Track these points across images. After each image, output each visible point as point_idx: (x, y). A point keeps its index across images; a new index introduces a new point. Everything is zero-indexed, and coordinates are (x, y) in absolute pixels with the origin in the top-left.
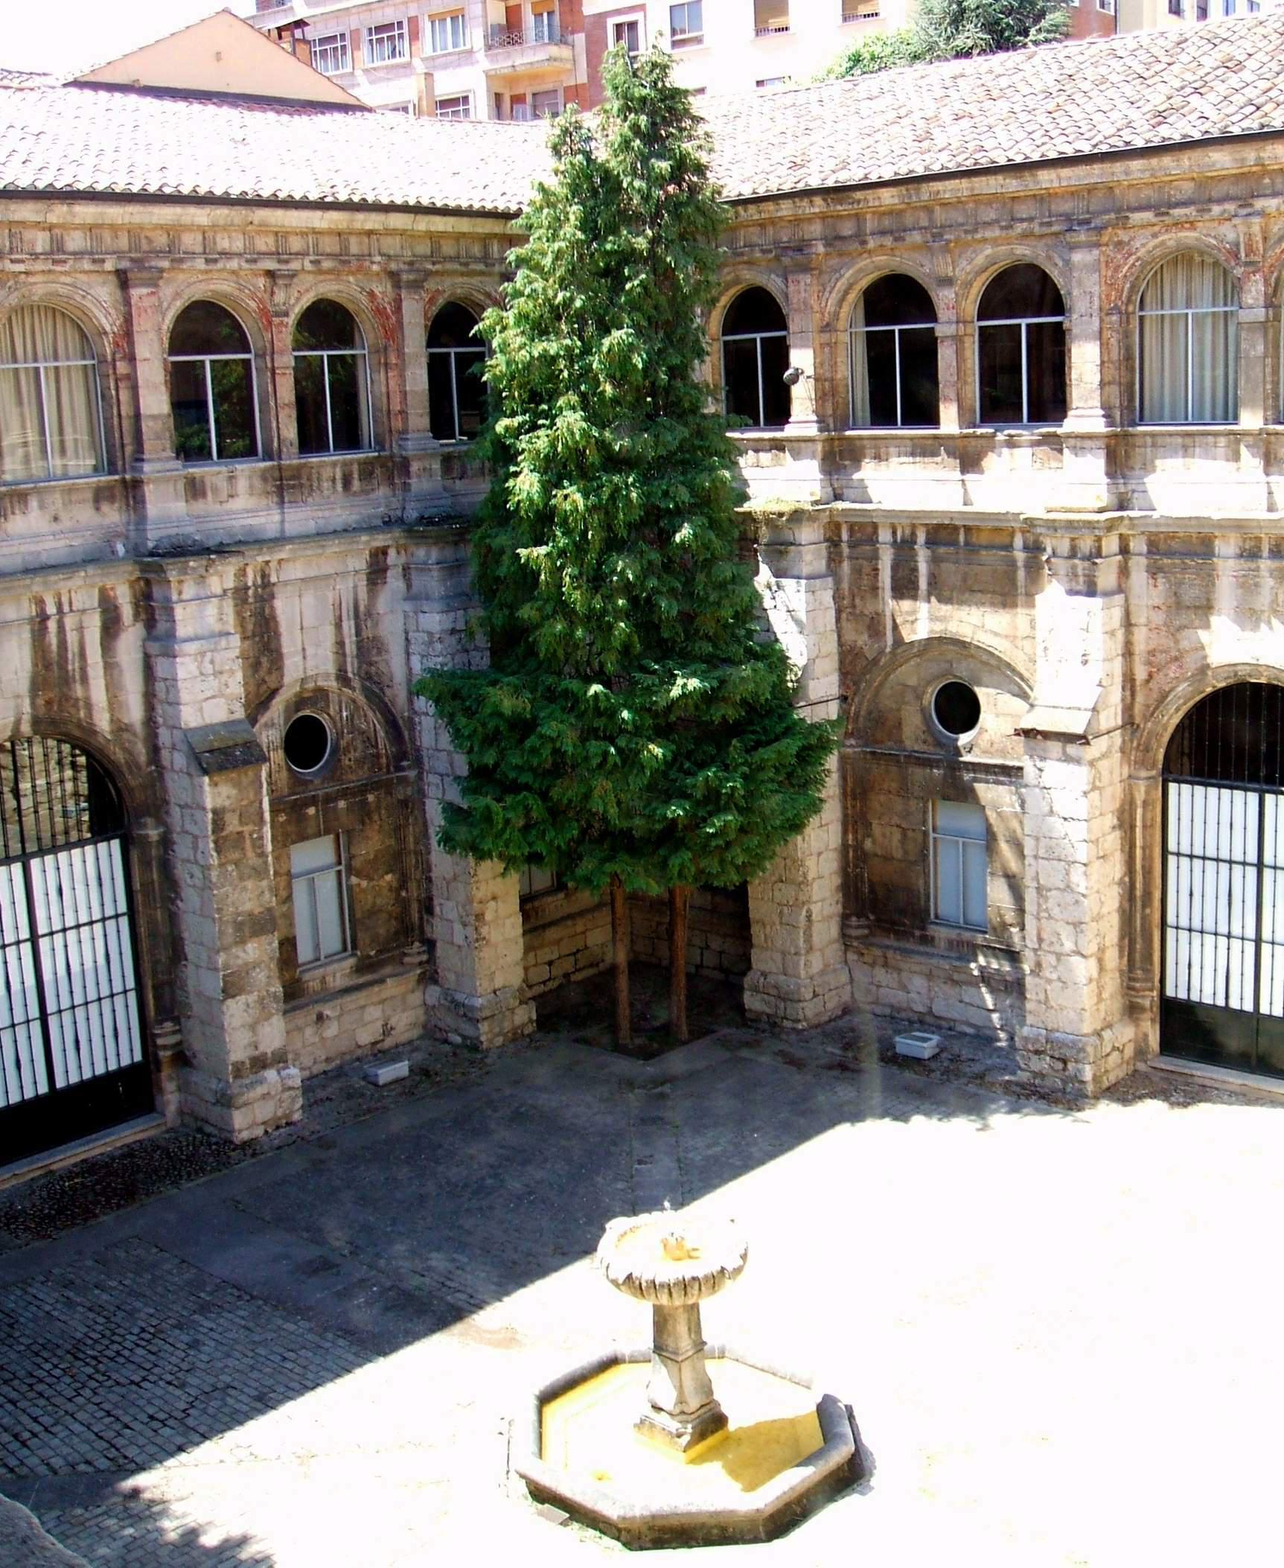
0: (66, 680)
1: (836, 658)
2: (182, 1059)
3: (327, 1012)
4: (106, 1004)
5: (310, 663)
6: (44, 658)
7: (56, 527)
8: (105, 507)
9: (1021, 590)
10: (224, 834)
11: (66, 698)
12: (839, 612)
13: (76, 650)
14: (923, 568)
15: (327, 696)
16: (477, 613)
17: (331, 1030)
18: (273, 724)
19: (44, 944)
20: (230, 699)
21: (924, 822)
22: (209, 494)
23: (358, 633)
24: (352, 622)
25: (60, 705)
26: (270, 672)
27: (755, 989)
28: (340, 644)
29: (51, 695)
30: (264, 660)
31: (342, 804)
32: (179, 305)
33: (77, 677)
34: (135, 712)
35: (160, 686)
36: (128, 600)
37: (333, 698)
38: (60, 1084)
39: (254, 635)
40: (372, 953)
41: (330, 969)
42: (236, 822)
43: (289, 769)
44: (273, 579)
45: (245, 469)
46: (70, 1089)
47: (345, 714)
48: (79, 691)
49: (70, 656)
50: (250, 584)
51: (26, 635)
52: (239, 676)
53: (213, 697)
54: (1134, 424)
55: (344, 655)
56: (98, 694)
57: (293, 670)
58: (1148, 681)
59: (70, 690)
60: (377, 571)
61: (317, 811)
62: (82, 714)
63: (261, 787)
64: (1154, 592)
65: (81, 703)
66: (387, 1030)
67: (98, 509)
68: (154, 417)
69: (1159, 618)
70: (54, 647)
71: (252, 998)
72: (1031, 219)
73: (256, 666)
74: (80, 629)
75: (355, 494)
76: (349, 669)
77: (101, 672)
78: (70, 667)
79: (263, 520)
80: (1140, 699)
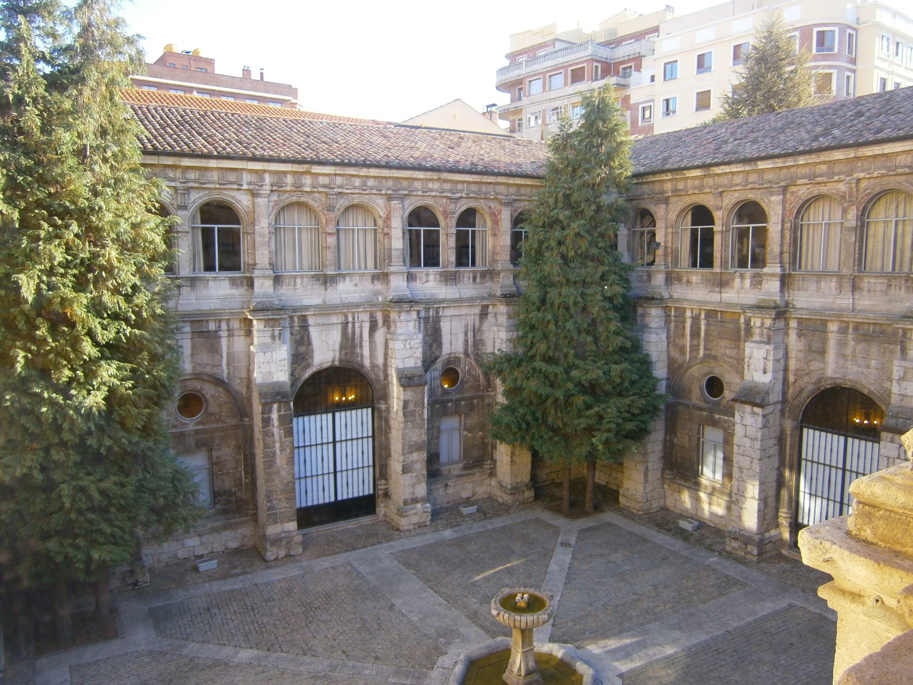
0: (353, 346)
2: (387, 495)
3: (450, 484)
5: (453, 347)
7: (355, 288)
8: (376, 282)
9: (742, 339)
11: (353, 353)
12: (668, 343)
14: (703, 327)
16: (515, 333)
17: (450, 491)
19: (338, 445)
21: (699, 434)
23: (474, 337)
27: (624, 496)
28: (466, 341)
32: (411, 208)
34: (380, 361)
35: (390, 351)
37: (462, 361)
38: (339, 498)
41: (452, 467)
45: (431, 270)
46: (343, 501)
48: (358, 350)
51: (340, 327)
52: (421, 350)
54: (795, 270)
56: (366, 352)
57: (446, 350)
58: (794, 383)
60: (484, 314)
64: (800, 344)
66: (474, 494)
69: (801, 355)
71: (414, 474)
72: (754, 183)
73: (431, 346)
74: (361, 327)
80: (791, 390)
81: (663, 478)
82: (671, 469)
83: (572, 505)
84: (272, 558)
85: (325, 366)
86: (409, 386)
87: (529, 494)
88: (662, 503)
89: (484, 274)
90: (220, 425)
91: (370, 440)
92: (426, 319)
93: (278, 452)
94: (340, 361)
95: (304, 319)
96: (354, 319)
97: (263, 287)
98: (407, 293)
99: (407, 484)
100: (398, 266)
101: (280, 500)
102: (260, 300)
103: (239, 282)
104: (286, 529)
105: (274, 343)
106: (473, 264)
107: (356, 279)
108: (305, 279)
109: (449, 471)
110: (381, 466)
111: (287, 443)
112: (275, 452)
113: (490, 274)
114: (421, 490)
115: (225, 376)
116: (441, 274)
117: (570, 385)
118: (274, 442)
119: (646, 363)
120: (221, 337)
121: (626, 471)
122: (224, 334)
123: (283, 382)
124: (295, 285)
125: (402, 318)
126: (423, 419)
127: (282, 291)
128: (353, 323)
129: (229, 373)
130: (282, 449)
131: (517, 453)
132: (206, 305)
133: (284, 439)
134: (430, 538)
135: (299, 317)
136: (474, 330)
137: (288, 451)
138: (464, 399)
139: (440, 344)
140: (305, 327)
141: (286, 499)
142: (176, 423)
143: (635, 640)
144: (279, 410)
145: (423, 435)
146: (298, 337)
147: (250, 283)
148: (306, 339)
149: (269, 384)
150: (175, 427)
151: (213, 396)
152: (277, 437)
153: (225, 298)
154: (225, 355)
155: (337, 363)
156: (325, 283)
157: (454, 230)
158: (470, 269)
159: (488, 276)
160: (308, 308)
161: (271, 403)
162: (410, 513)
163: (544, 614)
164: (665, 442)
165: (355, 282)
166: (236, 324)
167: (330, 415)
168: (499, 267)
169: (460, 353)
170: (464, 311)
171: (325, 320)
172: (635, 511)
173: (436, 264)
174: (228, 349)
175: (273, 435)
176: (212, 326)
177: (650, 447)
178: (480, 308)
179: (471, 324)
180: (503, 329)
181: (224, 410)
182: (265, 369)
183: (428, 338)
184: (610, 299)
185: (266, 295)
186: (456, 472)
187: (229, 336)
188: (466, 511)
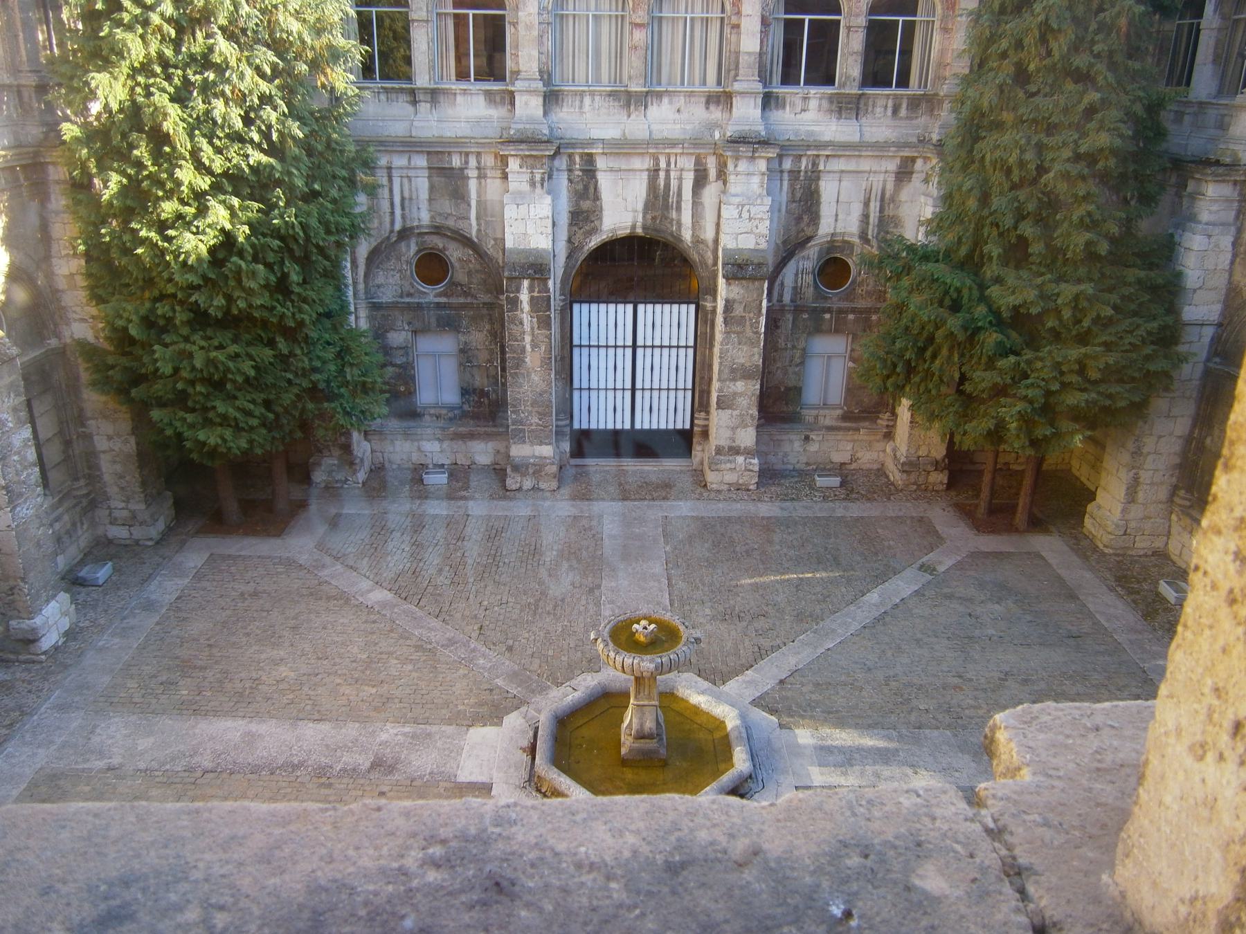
0: (666, 207)
1: (1224, 292)
2: (705, 434)
4: (672, 393)
7: (677, 116)
8: (712, 107)
11: (665, 217)
12: (1235, 256)
17: (813, 447)
19: (640, 352)
23: (882, 210)
24: (878, 204)
26: (808, 225)
28: (866, 217)
31: (851, 317)
34: (709, 235)
43: (816, 287)
44: (821, 167)
45: (813, 91)
46: (642, 431)
48: (674, 215)
51: (645, 175)
52: (767, 223)
55: (868, 224)
56: (686, 218)
57: (826, 227)
60: (904, 173)
66: (853, 459)
67: (707, 108)
68: (749, 54)
71: (737, 412)
73: (799, 219)
74: (680, 179)
75: (901, 118)
76: (870, 233)
79: (823, 128)
81: (1170, 500)
82: (1189, 490)
83: (992, 511)
85: (623, 233)
86: (735, 278)
87: (939, 478)
88: (1158, 544)
89: (914, 103)
90: (469, 300)
92: (794, 174)
93: (528, 348)
95: (589, 159)
96: (668, 164)
98: (761, 129)
99: (733, 426)
100: (748, 82)
102: (521, 126)
103: (498, 98)
104: (537, 454)
106: (904, 82)
107: (680, 101)
109: (816, 417)
110: (701, 392)
111: (541, 338)
112: (524, 347)
113: (926, 103)
114: (747, 437)
116: (831, 98)
117: (981, 310)
119: (1168, 291)
120: (469, 178)
121: (1103, 474)
122: (472, 173)
123: (544, 250)
124: (581, 107)
126: (757, 333)
127: (561, 115)
128: (668, 171)
129: (479, 230)
130: (535, 345)
132: (450, 131)
133: (537, 332)
134: (738, 508)
135: (581, 155)
136: (882, 199)
137: (543, 348)
138: (853, 311)
139: (815, 218)
140: (590, 172)
141: (539, 413)
142: (412, 291)
143: (881, 744)
144: (531, 289)
145: (757, 357)
146: (580, 187)
147: (511, 98)
148: (592, 190)
149: (523, 251)
151: (460, 260)
152: (527, 327)
153: (478, 121)
154: (473, 203)
155: (639, 231)
156: (628, 105)
157: (862, 21)
158: (893, 91)
160: (592, 142)
161: (521, 278)
163: (651, 661)
164: (1188, 440)
165: (677, 106)
166: (488, 160)
167: (630, 307)
168: (944, 90)
169: (852, 235)
170: (865, 165)
171: (622, 164)
172: (1101, 546)
173: (829, 80)
174: (479, 195)
175: (521, 323)
176: (456, 162)
177: (1149, 443)
178: (898, 161)
179: (877, 189)
180: (930, 201)
181: (475, 281)
184: (1091, 159)
185: (531, 120)
186: (828, 422)
187: (479, 177)
188: (820, 481)
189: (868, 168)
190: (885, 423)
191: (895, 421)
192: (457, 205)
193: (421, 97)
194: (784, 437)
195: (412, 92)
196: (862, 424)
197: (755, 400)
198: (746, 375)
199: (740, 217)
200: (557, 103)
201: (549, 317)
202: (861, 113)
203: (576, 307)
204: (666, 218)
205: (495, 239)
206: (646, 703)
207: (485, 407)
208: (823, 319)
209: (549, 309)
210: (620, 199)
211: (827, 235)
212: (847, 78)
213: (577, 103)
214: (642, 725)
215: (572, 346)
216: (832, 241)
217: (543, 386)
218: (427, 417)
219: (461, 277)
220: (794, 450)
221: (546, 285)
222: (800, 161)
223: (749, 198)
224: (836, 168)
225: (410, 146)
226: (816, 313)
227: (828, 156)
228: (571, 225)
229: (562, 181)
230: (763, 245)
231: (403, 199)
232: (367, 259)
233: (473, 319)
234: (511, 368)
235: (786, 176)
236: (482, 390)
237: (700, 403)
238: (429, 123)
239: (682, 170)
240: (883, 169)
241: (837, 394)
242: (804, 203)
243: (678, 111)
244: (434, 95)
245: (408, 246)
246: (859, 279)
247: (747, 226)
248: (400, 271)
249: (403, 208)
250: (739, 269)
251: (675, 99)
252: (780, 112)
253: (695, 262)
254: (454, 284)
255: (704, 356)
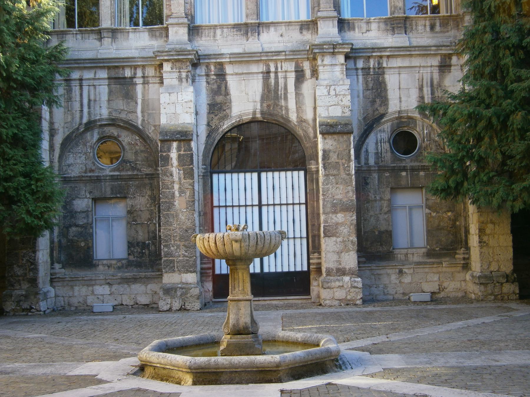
0: (277, 97)
6: (268, 88)
7: (281, 39)
8: (305, 32)
10: (329, 161)
11: (276, 105)
13: (283, 86)
15: (416, 122)
17: (407, 279)
18: (384, 131)
20: (344, 107)
22: (357, 30)
23: (433, 93)
24: (429, 89)
25: (273, 108)
26: (381, 106)
29: (270, 103)
30: (378, 100)
31: (422, 173)
33: (283, 97)
36: (309, 68)
37: (419, 123)
39: (372, 89)
40: (437, 249)
42: (335, 157)
43: (392, 152)
46: (269, 274)
47: (425, 132)
48: (283, 103)
49: (280, 88)
50: (372, 66)
51: (260, 76)
52: (349, 97)
53: (335, 105)
56: (292, 104)
57: (394, 106)
59: (279, 102)
60: (445, 67)
61: (407, 174)
62: (284, 112)
63: (350, 144)
65: (284, 108)
66: (441, 289)
67: (301, 33)
70: (273, 84)
71: (339, 240)
73: (373, 102)
74: (286, 78)
75: (437, 32)
77: (294, 96)
78: (279, 93)
84: (166, 308)
85: (247, 118)
91: (303, 207)
93: (177, 194)
94: (262, 113)
95: (221, 66)
96: (276, 68)
97: (178, 35)
99: (339, 252)
101: (178, 247)
103: (158, 34)
104: (184, 281)
105: (181, 85)
108: (225, 30)
110: (314, 236)
111: (187, 186)
112: (174, 193)
114: (351, 260)
115: (140, 122)
118: (173, 182)
120: (136, 84)
122: (139, 81)
124: (214, 36)
125: (325, 62)
126: (349, 175)
128: (276, 73)
129: (143, 120)
130: (181, 192)
131: (488, 231)
133: (183, 181)
137: (188, 193)
139: (385, 101)
140: (221, 76)
142: (93, 168)
144: (179, 149)
145: (351, 194)
146: (215, 87)
148: (223, 88)
150: (92, 171)
151: (129, 144)
152: (176, 178)
154: (140, 101)
159: (451, 23)
162: (333, 284)
170: (416, 62)
175: (172, 175)
176: (128, 73)
178: (439, 58)
179: (427, 78)
181: (140, 158)
182: (171, 109)
183: (368, 92)
186: (416, 259)
187: (144, 83)
189: (418, 65)
190: (461, 256)
191: (469, 253)
192: (128, 103)
193: (105, 34)
194: (382, 272)
195: (99, 32)
196: (443, 260)
197: (353, 229)
198: (345, 209)
199: (329, 94)
200: (198, 34)
201: (192, 169)
202: (408, 30)
203: (215, 176)
204: (277, 105)
205: (155, 126)
206: (241, 297)
207: (146, 257)
208: (401, 176)
209: (192, 163)
210: (244, 94)
211: (395, 112)
212: (395, 7)
213: (212, 34)
214: (238, 320)
215: (212, 207)
216: (400, 118)
217: (189, 224)
218: (101, 267)
219: (130, 156)
220: (391, 279)
221: (189, 145)
222: (369, 62)
223: (334, 81)
224: (395, 66)
225: (96, 64)
226: (395, 171)
227: (388, 57)
228: (209, 113)
229: (203, 83)
230: (348, 114)
231: (89, 101)
232: (62, 144)
233: (138, 187)
234: (164, 210)
235: (360, 72)
236: (144, 243)
237: (314, 247)
238: (109, 49)
239: (286, 71)
240: (429, 65)
241: (420, 238)
242: (377, 90)
243: (281, 36)
244: (114, 32)
245: (92, 136)
246: (424, 145)
247: (335, 100)
248: (85, 153)
249: (89, 107)
250: (331, 129)
251: (279, 28)
252: (352, 33)
253: (301, 137)
254: (124, 161)
255: (314, 208)
